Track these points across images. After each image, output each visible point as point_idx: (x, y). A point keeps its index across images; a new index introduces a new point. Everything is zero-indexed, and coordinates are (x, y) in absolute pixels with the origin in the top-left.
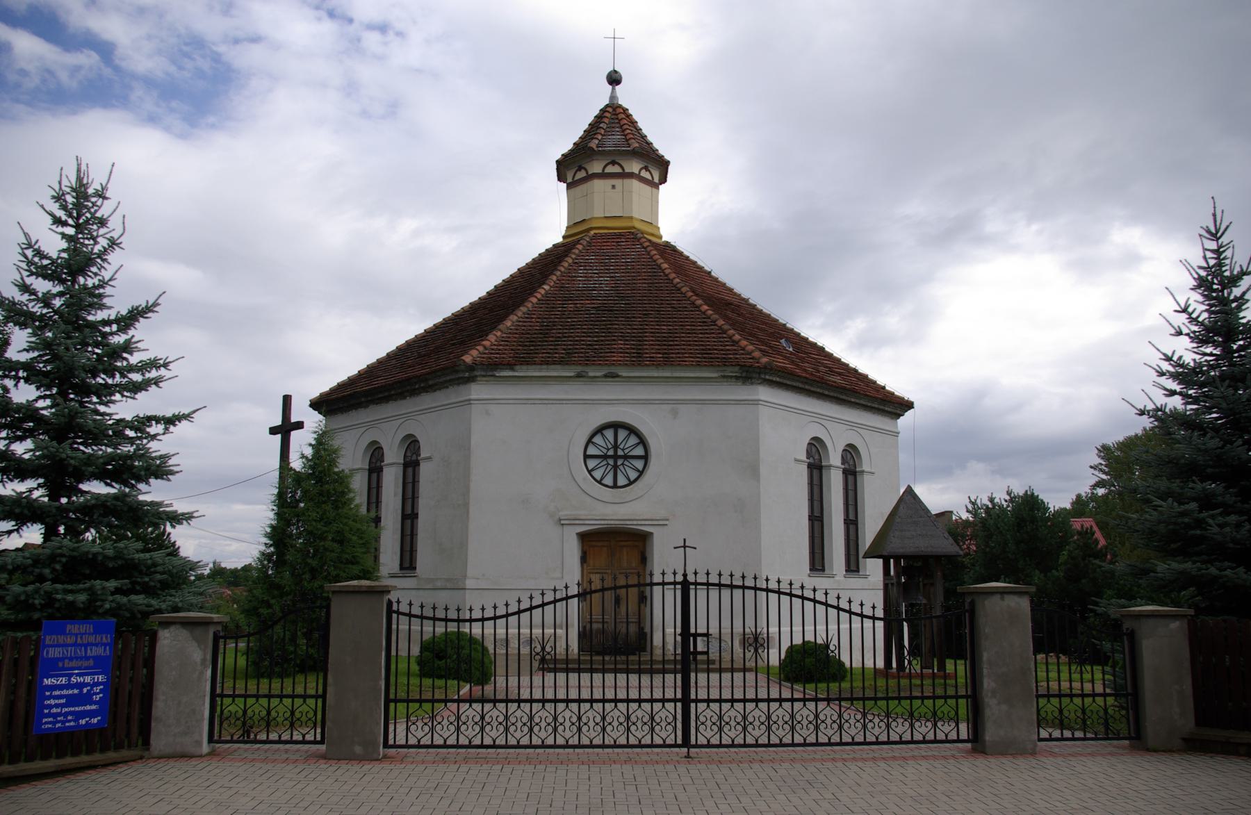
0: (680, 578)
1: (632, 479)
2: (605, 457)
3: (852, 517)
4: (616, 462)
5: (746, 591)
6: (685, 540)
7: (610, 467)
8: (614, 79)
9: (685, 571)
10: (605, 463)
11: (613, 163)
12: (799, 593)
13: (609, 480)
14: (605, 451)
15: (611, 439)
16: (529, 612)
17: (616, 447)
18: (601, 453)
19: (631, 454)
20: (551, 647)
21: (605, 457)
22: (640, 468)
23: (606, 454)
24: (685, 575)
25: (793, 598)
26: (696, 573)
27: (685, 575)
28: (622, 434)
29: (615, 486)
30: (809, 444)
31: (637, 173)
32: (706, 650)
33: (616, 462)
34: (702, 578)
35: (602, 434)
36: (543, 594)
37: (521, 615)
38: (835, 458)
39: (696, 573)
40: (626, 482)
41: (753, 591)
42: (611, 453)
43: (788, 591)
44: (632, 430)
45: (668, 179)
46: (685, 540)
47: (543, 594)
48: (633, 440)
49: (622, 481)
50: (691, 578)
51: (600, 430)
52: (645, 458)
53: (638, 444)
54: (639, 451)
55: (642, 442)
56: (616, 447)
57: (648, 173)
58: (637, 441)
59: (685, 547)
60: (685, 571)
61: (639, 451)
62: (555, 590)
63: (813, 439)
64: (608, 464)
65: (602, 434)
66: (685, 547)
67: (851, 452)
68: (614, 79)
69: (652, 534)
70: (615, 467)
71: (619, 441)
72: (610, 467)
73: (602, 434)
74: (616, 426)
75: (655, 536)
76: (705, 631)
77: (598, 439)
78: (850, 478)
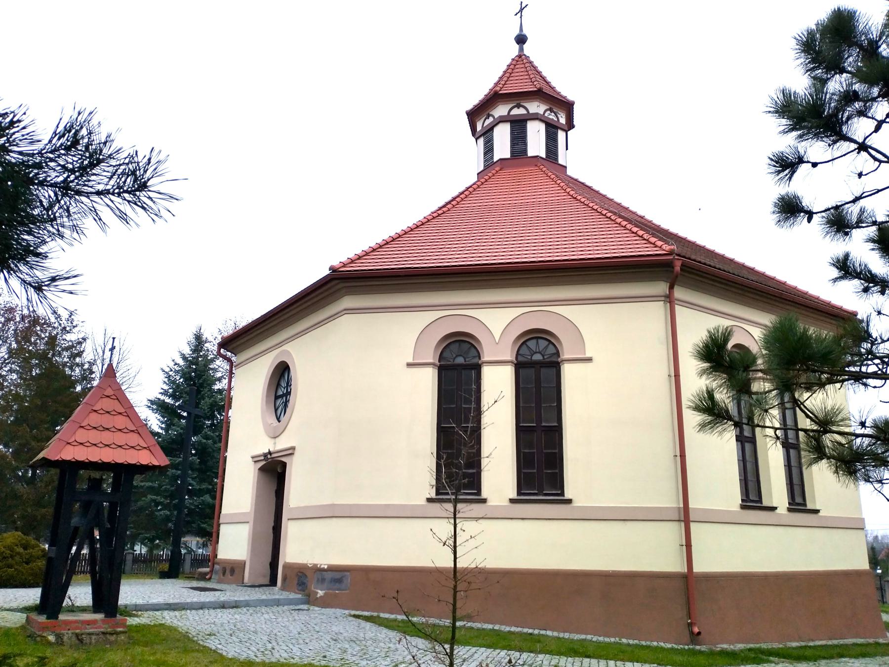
11: (518, 106)
68: (521, 40)
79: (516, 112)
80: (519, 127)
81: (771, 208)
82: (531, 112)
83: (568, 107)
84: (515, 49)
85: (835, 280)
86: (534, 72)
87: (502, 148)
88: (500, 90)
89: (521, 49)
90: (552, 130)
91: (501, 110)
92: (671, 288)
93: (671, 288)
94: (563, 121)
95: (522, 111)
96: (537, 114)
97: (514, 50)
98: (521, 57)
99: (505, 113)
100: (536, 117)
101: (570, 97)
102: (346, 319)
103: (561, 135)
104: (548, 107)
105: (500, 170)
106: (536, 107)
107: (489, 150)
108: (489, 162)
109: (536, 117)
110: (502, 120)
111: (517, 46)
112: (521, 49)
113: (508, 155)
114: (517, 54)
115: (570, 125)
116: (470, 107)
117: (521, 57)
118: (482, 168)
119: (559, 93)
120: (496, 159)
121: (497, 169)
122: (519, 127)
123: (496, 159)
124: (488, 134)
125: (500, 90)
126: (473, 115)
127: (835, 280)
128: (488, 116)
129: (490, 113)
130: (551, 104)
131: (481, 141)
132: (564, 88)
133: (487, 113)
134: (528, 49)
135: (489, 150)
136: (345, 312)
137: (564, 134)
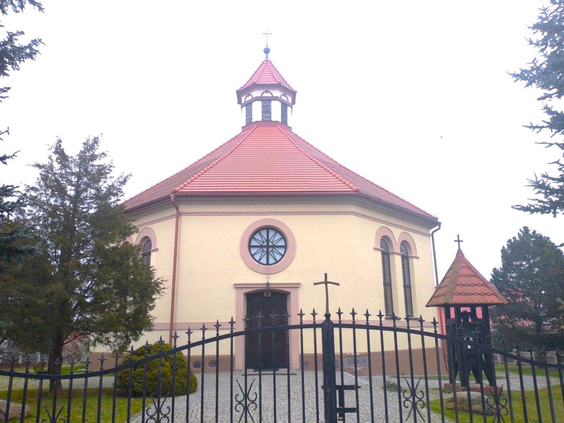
0: (320, 318)
1: (278, 260)
2: (261, 247)
3: (407, 284)
4: (268, 250)
5: (371, 331)
6: (326, 275)
7: (264, 253)
8: (267, 51)
9: (327, 310)
10: (261, 250)
11: (267, 92)
12: (432, 330)
13: (264, 261)
14: (261, 243)
15: (265, 236)
16: (201, 346)
17: (268, 240)
18: (259, 244)
19: (276, 245)
20: (168, 408)
21: (261, 247)
22: (283, 253)
23: (262, 245)
24: (328, 316)
25: (425, 337)
26: (340, 313)
27: (328, 316)
28: (272, 233)
29: (268, 264)
30: (381, 239)
31: (280, 97)
32: (355, 406)
33: (268, 250)
34: (347, 318)
35: (260, 233)
36: (189, 333)
37: (206, 345)
38: (397, 248)
39: (340, 313)
40: (274, 261)
41: (379, 331)
42: (265, 249)
43: (419, 329)
44: (277, 231)
45: (296, 102)
46: (326, 275)
47: (189, 333)
48: (278, 236)
49: (271, 261)
50: (334, 318)
51: (258, 231)
52: (285, 247)
53: (281, 238)
54: (282, 243)
55: (284, 237)
56: (268, 240)
57: (285, 97)
58: (280, 237)
59: (326, 283)
60: (327, 310)
61: (282, 243)
62: (204, 329)
63: (383, 237)
64: (263, 251)
65: (260, 233)
66: (326, 283)
67: (405, 245)
68: (267, 51)
69: (289, 293)
70: (268, 253)
71: (270, 237)
72: (264, 253)
73: (260, 233)
74: (268, 228)
75: (291, 293)
76: (353, 383)
77: (257, 236)
78: (405, 260)
79: (265, 95)
80: (266, 102)
81: (263, 49)
82: (274, 95)
83: (293, 94)
84: (263, 57)
85: (537, 40)
86: (275, 71)
87: (257, 116)
88: (257, 82)
89: (267, 57)
90: (285, 106)
91: (257, 93)
92: (177, 209)
93: (177, 209)
94: (290, 101)
95: (268, 95)
96: (277, 97)
97: (263, 57)
98: (267, 63)
99: (260, 95)
100: (276, 99)
101: (295, 88)
102: (353, 217)
103: (289, 109)
104: (283, 93)
105: (257, 127)
106: (277, 93)
107: (249, 114)
108: (249, 122)
109: (276, 99)
110: (257, 99)
111: (265, 55)
112: (267, 57)
113: (260, 119)
114: (265, 59)
115: (294, 102)
116: (238, 88)
117: (267, 63)
118: (245, 125)
119: (289, 85)
120: (253, 121)
121: (255, 127)
122: (266, 102)
123: (253, 121)
124: (248, 105)
125: (257, 82)
126: (240, 93)
127: (537, 40)
128: (249, 95)
129: (250, 94)
130: (284, 92)
131: (244, 108)
132: (293, 83)
133: (248, 93)
134: (271, 57)
135: (249, 114)
136: (353, 214)
137: (291, 108)
